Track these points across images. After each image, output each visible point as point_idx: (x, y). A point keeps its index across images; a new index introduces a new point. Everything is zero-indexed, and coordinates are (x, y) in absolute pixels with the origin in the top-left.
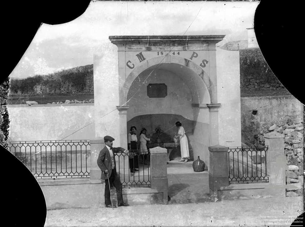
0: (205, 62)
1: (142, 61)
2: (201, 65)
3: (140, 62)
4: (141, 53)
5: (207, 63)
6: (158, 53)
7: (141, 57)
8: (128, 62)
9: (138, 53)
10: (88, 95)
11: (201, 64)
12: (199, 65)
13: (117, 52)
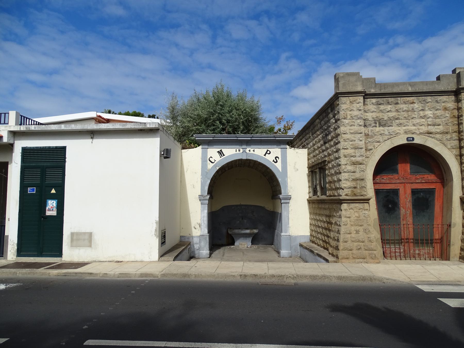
0: (275, 161)
1: (222, 156)
2: (273, 161)
3: (221, 157)
4: (221, 150)
5: (274, 160)
6: (236, 150)
7: (221, 153)
8: (210, 158)
9: (219, 150)
11: (274, 160)
12: (272, 161)
13: (201, 149)
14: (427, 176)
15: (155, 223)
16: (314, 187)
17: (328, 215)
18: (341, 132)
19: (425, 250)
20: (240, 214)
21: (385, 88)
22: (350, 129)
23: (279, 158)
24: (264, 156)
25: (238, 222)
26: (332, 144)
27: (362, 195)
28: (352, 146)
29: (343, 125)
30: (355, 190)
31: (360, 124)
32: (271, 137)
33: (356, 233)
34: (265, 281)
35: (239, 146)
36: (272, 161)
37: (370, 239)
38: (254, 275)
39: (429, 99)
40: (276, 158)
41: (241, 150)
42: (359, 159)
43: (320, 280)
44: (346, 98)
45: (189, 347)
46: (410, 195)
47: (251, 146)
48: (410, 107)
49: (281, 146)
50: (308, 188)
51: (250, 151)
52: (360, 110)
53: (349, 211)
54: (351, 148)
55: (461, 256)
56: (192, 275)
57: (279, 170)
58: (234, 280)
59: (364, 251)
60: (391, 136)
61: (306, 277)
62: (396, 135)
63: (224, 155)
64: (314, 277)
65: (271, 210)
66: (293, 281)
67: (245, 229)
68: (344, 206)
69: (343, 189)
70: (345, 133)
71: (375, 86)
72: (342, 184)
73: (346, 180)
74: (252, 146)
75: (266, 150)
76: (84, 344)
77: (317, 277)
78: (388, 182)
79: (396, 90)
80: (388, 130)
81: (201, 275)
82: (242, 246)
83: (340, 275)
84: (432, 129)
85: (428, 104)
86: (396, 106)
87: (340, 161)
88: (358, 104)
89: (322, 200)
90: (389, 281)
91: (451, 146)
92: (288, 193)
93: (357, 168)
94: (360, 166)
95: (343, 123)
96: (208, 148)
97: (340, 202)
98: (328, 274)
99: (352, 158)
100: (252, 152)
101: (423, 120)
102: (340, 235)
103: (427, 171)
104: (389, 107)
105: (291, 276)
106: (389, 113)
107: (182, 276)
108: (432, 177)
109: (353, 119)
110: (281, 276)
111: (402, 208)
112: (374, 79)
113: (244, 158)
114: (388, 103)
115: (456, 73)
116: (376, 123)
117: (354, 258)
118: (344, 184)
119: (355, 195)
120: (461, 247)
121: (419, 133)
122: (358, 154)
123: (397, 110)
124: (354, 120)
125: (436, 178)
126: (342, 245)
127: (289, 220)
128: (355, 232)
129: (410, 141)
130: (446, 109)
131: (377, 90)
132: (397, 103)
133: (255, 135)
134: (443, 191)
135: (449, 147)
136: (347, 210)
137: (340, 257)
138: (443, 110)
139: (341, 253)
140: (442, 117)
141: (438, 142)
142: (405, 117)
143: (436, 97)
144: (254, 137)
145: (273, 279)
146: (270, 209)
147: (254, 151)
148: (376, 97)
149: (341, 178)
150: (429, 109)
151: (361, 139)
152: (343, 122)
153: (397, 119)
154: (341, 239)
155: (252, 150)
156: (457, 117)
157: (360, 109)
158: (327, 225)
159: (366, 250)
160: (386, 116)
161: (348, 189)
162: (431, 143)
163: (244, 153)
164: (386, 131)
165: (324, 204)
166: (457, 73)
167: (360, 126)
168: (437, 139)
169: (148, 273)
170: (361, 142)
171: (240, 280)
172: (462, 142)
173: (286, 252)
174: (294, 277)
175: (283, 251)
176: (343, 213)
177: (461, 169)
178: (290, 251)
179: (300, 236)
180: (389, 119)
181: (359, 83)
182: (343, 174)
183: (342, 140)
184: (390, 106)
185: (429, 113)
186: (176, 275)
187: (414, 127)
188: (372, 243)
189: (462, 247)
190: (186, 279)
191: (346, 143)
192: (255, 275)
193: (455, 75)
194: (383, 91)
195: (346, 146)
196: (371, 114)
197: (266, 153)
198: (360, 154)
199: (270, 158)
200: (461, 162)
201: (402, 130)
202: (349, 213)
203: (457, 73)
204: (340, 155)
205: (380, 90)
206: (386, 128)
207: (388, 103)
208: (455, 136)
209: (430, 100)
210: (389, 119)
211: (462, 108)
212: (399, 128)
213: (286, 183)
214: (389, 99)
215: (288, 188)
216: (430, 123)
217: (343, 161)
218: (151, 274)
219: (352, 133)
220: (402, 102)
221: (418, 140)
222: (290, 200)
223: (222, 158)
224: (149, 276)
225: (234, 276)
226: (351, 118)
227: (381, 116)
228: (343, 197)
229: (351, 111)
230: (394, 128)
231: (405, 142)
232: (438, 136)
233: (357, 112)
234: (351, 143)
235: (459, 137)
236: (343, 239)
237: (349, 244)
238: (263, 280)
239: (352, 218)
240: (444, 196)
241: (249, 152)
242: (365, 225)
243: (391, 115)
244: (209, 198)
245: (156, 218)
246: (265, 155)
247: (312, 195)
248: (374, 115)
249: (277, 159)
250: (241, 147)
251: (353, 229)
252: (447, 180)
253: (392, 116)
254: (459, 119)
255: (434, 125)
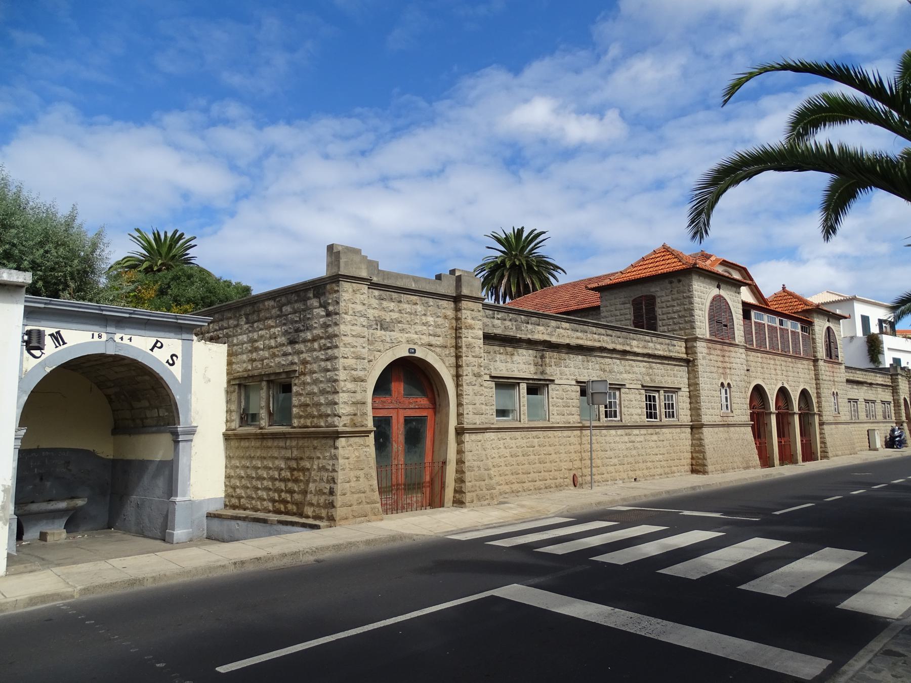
0: (171, 362)
2: (167, 362)
3: (57, 347)
4: (58, 333)
5: (168, 360)
6: (93, 334)
10: (747, 361)
11: (168, 360)
12: (164, 362)
14: (421, 399)
15: (2, 491)
16: (242, 411)
17: (296, 458)
18: (340, 333)
19: (416, 497)
20: (36, 470)
21: (388, 278)
22: (351, 330)
23: (177, 357)
24: (150, 352)
25: (31, 487)
26: (315, 347)
27: (363, 426)
28: (353, 354)
29: (344, 322)
30: (355, 418)
31: (364, 324)
32: (150, 316)
33: (356, 480)
34: (273, 566)
35: (100, 327)
36: (164, 362)
37: (372, 487)
38: (257, 558)
39: (431, 302)
40: (172, 356)
41: (105, 337)
42: (361, 374)
43: (345, 549)
44: (348, 283)
45: (337, 638)
46: (403, 426)
47: (124, 330)
48: (413, 309)
49: (183, 335)
50: (225, 413)
51: (122, 338)
52: (364, 304)
53: (347, 448)
54: (351, 357)
55: (455, 499)
56: (148, 579)
57: (177, 380)
58: (225, 573)
59: (366, 506)
60: (395, 344)
61: (328, 548)
62: (398, 344)
63: (64, 343)
64: (337, 547)
65: (108, 457)
66: (311, 559)
67: (47, 501)
68: (342, 442)
69: (340, 417)
70: (345, 335)
71: (378, 273)
72: (339, 409)
73: (345, 403)
74: (128, 331)
75: (154, 340)
76: (217, 669)
77: (342, 546)
78: (381, 406)
79: (399, 284)
80: (390, 336)
81: (165, 575)
82: (54, 537)
83: (368, 538)
84: (433, 340)
85: (429, 308)
86: (399, 304)
87: (336, 375)
88: (361, 296)
89: (273, 433)
90: (418, 537)
91: (449, 364)
92: (192, 422)
93: (358, 387)
94: (362, 383)
95: (343, 320)
96: (27, 325)
97: (336, 435)
98: (353, 540)
99: (353, 372)
100: (126, 341)
101: (425, 328)
102: (335, 485)
103: (420, 394)
104: (392, 305)
105: (308, 550)
106: (391, 314)
107: (126, 585)
108: (424, 401)
109: (356, 316)
110: (295, 553)
111: (394, 443)
112: (377, 263)
113: (111, 351)
114: (391, 299)
115: (455, 275)
116: (377, 325)
117: (354, 517)
118: (343, 409)
119: (355, 425)
120: (455, 488)
121: (420, 344)
122: (359, 367)
123: (400, 310)
124: (356, 317)
125: (428, 402)
126: (340, 499)
127: (191, 472)
128: (355, 479)
129: (412, 353)
130: (445, 317)
131: (380, 278)
132: (400, 302)
133: (183, 315)
134: (435, 420)
135: (447, 365)
136: (345, 447)
137: (337, 518)
138: (443, 318)
139: (339, 512)
140: (442, 327)
141: (438, 358)
142: (408, 321)
143: (437, 300)
144: (136, 312)
145: (285, 560)
146: (108, 456)
147: (130, 339)
148: (348, 280)
149: (339, 400)
150: (431, 314)
151: (364, 345)
152: (344, 319)
153: (400, 322)
154: (338, 491)
155: (126, 338)
156: (455, 328)
157: (364, 302)
158: (289, 474)
159: (368, 503)
160: (388, 316)
161: (347, 417)
162: (431, 358)
163: (111, 342)
164: (388, 337)
165: (281, 440)
166: (456, 275)
167: (364, 326)
168: (437, 354)
169: (43, 593)
170: (363, 350)
171: (235, 571)
172: (460, 359)
173: (184, 532)
174: (312, 551)
175: (179, 532)
176: (341, 452)
177: (457, 392)
178: (191, 530)
179: (208, 499)
180: (391, 321)
181: (363, 266)
182: (341, 395)
183: (342, 344)
184: (393, 304)
185: (430, 319)
186: (114, 585)
187: (416, 336)
188: (374, 493)
189: (456, 488)
190: (137, 588)
191: (347, 349)
192: (258, 559)
193: (454, 277)
194: (386, 282)
195: (346, 354)
196: (372, 311)
197: (155, 346)
198: (362, 367)
199: (162, 355)
200: (457, 384)
201: (404, 338)
202: (347, 452)
203: (456, 275)
204: (338, 367)
205: (383, 279)
206: (388, 332)
207: (391, 300)
208: (453, 350)
209: (432, 304)
210: (391, 321)
211: (461, 320)
212: (402, 335)
213: (188, 403)
214: (393, 294)
215: (192, 414)
216: (431, 333)
217: (342, 375)
218: (55, 594)
219: (353, 336)
220: (405, 301)
221: (418, 354)
222: (194, 434)
223: (60, 348)
224: (51, 598)
225: (223, 566)
226: (353, 314)
227: (383, 315)
228: (341, 429)
229: (353, 303)
230: (396, 335)
231: (407, 354)
232: (438, 350)
233: (361, 306)
234: (352, 350)
235: (456, 354)
236: (341, 491)
237: (349, 498)
238: (270, 565)
239: (351, 459)
240: (436, 426)
241: (120, 341)
242: (366, 468)
243: (395, 315)
244: (24, 436)
245: (5, 479)
246: (152, 350)
247: (237, 426)
248: (376, 313)
249: (174, 358)
250: (104, 330)
251: (353, 475)
252: (440, 405)
253: (395, 317)
254: (458, 331)
255: (435, 336)
